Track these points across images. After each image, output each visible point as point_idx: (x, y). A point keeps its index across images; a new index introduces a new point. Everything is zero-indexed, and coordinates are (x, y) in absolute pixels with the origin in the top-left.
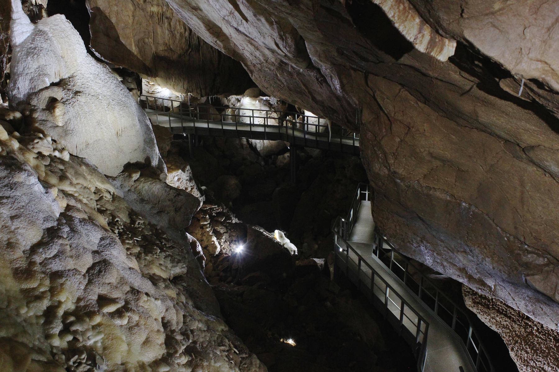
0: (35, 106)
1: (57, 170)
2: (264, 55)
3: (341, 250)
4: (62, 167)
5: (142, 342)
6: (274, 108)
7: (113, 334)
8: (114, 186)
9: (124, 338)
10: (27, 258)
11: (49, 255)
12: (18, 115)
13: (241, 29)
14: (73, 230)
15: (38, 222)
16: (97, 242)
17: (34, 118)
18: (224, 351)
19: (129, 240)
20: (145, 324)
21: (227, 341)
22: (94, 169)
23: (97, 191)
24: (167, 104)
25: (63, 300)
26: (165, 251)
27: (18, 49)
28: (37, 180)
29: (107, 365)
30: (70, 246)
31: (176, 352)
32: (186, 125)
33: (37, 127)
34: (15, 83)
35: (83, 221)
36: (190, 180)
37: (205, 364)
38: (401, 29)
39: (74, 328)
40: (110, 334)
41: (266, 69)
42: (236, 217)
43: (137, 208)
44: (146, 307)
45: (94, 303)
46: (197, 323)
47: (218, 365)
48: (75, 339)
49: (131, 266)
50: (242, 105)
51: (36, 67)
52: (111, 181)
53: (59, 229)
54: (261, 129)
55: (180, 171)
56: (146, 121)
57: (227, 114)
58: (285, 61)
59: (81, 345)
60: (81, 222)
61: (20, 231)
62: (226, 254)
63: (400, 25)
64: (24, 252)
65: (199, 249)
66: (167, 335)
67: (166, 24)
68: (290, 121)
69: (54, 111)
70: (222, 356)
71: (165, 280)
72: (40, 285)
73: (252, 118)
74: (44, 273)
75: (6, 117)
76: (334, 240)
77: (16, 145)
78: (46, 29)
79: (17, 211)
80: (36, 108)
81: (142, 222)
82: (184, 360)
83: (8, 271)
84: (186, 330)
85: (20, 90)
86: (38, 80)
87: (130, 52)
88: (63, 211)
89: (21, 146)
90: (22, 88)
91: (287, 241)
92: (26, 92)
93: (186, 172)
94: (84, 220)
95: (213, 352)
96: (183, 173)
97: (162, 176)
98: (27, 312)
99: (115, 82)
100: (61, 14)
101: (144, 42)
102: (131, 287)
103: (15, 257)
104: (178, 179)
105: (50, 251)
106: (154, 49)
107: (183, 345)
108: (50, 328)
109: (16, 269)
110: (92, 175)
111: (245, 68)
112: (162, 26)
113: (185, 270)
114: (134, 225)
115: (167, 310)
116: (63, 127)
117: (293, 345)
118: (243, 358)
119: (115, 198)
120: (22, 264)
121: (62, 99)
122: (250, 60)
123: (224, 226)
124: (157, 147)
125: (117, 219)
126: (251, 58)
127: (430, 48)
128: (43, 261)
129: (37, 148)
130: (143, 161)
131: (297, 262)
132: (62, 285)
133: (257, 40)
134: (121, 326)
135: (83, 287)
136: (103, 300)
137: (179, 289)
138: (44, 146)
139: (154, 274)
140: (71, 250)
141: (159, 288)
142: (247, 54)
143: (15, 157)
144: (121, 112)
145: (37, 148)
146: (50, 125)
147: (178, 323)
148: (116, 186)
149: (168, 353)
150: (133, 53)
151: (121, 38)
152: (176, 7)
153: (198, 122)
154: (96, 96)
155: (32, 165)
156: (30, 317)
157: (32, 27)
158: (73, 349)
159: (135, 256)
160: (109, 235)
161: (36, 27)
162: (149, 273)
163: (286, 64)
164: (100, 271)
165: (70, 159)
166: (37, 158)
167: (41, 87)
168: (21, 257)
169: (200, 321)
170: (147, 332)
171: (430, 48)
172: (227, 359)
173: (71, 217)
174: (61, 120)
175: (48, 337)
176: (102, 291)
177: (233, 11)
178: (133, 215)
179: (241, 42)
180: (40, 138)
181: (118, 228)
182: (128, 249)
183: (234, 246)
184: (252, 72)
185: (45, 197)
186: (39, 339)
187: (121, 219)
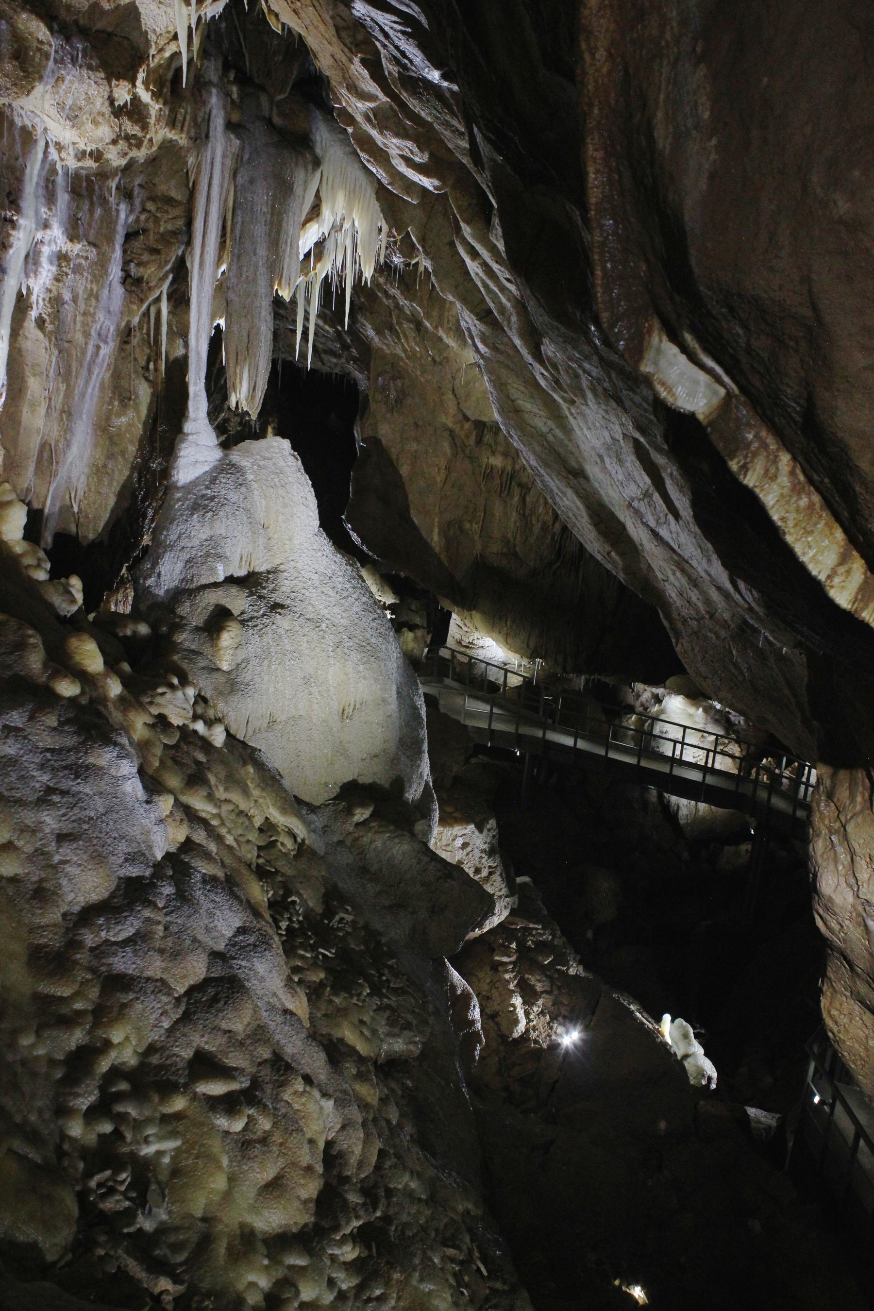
0: (182, 618)
1: (187, 761)
2: (708, 601)
3: (817, 1099)
4: (201, 757)
5: (263, 1183)
6: (736, 732)
7: (203, 1145)
8: (307, 824)
9: (225, 1161)
10: (67, 929)
11: (114, 936)
12: (143, 629)
13: (663, 532)
14: (183, 897)
15: (112, 859)
16: (229, 933)
17: (175, 642)
18: (452, 1260)
19: (306, 951)
20: (281, 1144)
21: (467, 1239)
22: (273, 778)
23: (268, 827)
24: (494, 675)
25: (116, 1040)
26: (381, 996)
27: (178, 495)
28: (135, 770)
29: (170, 1212)
30: (166, 928)
31: (336, 1228)
32: (525, 730)
33: (174, 663)
34: (155, 564)
35: (210, 881)
36: (491, 853)
37: (396, 1276)
38: (798, 549)
39: (120, 1108)
40: (196, 1143)
41: (709, 634)
42: (580, 962)
43: (347, 885)
44: (296, 1106)
45: (181, 1065)
46: (406, 1178)
47: (427, 1287)
48: (117, 1134)
49: (290, 1006)
50: (663, 711)
51: (204, 537)
52: (304, 812)
53: (153, 885)
54: (695, 776)
55: (472, 827)
56: (416, 698)
57: (625, 724)
58: (751, 622)
59: (125, 1149)
60: (204, 882)
61: (68, 868)
62: (536, 1042)
63: (797, 540)
64: (64, 915)
65: (476, 1014)
66: (327, 1185)
67: (516, 499)
68: (767, 770)
69: (218, 638)
70: (442, 1269)
71: (361, 1060)
72: (77, 994)
73: (679, 746)
74: (93, 970)
75: (118, 630)
76: (806, 1072)
77: (115, 688)
78: (245, 463)
79: (75, 824)
80: (184, 622)
81: (349, 918)
82: (349, 1253)
83: (18, 948)
84: (375, 1186)
85: (162, 578)
86: (203, 564)
87: (425, 546)
88: (173, 850)
89: (126, 692)
90: (168, 573)
91: (698, 1049)
92: (172, 585)
93: (485, 832)
94: (214, 879)
95: (424, 1252)
96: (477, 832)
97: (419, 827)
98: (33, 1046)
99: (364, 599)
100: (283, 437)
101: (461, 529)
102: (274, 1053)
103: (44, 921)
104: (459, 843)
105: (119, 928)
106: (479, 547)
107: (357, 1217)
108: (71, 1094)
109: (38, 948)
110: (263, 789)
111: (665, 623)
112: (505, 501)
113: (416, 1050)
114: (330, 921)
115: (343, 1127)
116: (229, 673)
117: (641, 1302)
118: (494, 1291)
119: (302, 849)
120: (52, 940)
121: (242, 613)
122: (677, 608)
123: (547, 976)
124: (426, 756)
125: (293, 898)
126: (679, 602)
127: (861, 600)
128: (100, 946)
129: (158, 705)
130: (387, 785)
131: (702, 1102)
132: (124, 1006)
133: (694, 563)
134: (227, 1133)
135: (166, 1025)
136: (205, 1065)
137: (392, 1090)
138: (176, 705)
139: (341, 1040)
140: (165, 937)
141: (341, 1073)
142: (672, 593)
143: (105, 712)
144: (361, 668)
145: (158, 705)
146: (203, 663)
147: (361, 1164)
148: (313, 826)
149: (316, 1224)
150: (432, 549)
151: (412, 511)
152: (533, 463)
153: (554, 730)
154: (316, 622)
155: (136, 737)
156: (37, 1058)
157: (218, 454)
158: (106, 1154)
159: (309, 987)
160: (258, 926)
161: (226, 455)
162: (329, 1034)
163: (755, 631)
164: (215, 1000)
165: (226, 744)
166: (152, 726)
167: (204, 581)
168: (55, 925)
169: (419, 1176)
170: (281, 1163)
171: (861, 600)
172: (452, 1281)
173: (188, 866)
174: (228, 657)
175: (62, 1111)
176: (206, 1043)
177: (650, 491)
178: (333, 897)
179: (661, 563)
180: (172, 687)
181: (290, 919)
182: (296, 970)
183: (560, 1030)
184: (678, 635)
185: (142, 811)
186: (40, 1111)
187: (304, 902)
